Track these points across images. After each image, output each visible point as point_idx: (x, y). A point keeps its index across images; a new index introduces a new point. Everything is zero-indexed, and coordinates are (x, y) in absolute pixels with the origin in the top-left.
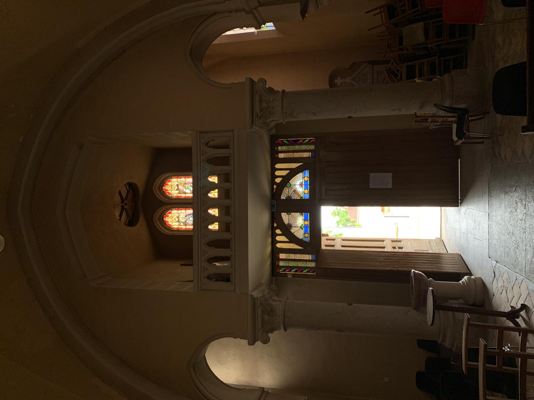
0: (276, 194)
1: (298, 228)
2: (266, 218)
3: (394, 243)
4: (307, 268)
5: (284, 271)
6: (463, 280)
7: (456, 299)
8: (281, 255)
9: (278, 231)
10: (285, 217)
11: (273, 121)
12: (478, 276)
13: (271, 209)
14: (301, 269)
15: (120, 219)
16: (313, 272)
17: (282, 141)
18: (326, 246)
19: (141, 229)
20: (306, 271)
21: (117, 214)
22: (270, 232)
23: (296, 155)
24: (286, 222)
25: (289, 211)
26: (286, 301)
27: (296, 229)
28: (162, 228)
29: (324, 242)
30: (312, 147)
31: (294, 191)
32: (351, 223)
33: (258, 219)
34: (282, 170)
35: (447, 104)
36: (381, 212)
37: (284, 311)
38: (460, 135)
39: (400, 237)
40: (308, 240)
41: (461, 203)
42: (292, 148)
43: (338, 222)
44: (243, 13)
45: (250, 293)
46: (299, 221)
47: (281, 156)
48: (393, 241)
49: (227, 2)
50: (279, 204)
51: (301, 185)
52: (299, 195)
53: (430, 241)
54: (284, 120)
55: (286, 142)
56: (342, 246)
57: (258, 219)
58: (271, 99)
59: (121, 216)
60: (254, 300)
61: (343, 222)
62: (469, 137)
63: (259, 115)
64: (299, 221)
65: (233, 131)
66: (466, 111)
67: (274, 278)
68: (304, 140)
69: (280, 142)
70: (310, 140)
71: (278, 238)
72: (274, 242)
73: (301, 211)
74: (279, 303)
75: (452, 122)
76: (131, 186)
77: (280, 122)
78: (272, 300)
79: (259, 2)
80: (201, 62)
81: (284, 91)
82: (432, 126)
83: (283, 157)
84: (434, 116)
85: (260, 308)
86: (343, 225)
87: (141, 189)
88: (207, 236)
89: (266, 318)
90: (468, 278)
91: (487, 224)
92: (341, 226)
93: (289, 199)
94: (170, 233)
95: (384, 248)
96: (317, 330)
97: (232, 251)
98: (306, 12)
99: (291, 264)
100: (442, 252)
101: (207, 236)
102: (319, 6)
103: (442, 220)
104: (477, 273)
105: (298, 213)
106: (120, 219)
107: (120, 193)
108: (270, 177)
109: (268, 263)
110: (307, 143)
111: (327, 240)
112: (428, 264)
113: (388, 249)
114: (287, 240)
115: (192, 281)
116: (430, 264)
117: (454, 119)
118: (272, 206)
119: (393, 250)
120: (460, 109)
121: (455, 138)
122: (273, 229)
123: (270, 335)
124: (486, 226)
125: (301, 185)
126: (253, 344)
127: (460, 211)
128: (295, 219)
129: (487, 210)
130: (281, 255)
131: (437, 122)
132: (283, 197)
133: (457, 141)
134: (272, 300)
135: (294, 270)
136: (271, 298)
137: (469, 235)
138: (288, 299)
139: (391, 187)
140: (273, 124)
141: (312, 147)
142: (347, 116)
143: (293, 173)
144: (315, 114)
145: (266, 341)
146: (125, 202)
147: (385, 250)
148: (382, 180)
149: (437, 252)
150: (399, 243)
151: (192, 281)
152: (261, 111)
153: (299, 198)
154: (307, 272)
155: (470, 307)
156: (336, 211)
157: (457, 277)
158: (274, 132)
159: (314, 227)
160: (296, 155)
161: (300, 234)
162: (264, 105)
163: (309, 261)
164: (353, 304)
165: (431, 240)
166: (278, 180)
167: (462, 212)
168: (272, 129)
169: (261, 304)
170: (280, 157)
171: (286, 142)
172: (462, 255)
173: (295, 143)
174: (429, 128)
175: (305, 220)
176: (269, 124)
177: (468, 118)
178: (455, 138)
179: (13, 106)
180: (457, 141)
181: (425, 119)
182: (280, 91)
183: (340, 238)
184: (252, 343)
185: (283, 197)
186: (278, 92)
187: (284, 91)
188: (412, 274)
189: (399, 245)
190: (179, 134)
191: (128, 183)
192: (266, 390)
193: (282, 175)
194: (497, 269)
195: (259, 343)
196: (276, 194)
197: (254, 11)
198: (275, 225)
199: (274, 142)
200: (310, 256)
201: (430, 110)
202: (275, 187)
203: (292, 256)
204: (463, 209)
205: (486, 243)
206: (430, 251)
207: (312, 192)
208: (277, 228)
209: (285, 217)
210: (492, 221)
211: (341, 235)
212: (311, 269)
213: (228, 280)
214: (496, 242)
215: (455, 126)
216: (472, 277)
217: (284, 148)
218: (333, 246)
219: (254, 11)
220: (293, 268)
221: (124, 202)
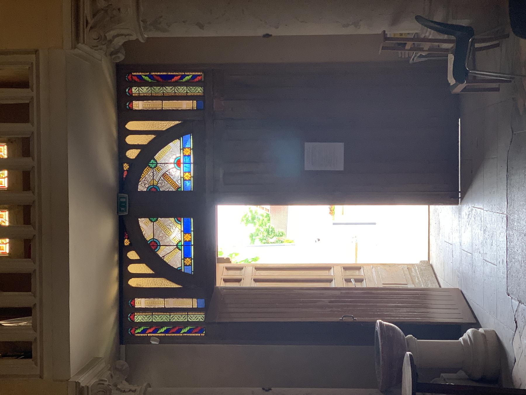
0: (126, 182)
1: (172, 248)
2: (106, 229)
3: (348, 273)
4: (188, 323)
5: (144, 332)
6: (465, 336)
7: (454, 370)
8: (137, 300)
9: (132, 255)
10: (146, 226)
11: (118, 36)
12: (490, 328)
13: (119, 210)
14: (178, 326)
17: (140, 77)
18: (226, 281)
20: (185, 330)
22: (116, 257)
23: (168, 105)
24: (148, 235)
25: (154, 215)
26: (146, 389)
27: (167, 249)
29: (221, 273)
30: (199, 90)
31: (164, 175)
32: (272, 236)
33: (89, 233)
34: (139, 133)
35: (439, 17)
36: (330, 215)
38: (461, 74)
39: (360, 261)
40: (190, 270)
41: (462, 198)
42: (158, 90)
43: (252, 236)
45: (73, 378)
47: (138, 105)
48: (346, 268)
50: (132, 204)
51: (178, 163)
52: (173, 183)
53: (410, 267)
54: (142, 35)
55: (147, 78)
56: (256, 280)
57: (89, 233)
61: (261, 236)
62: (475, 79)
63: (91, 22)
65: (36, 52)
66: (469, 31)
67: (123, 347)
68: (183, 77)
69: (136, 79)
70: (194, 77)
71: (132, 268)
72: (124, 276)
73: (177, 215)
75: (447, 50)
77: (133, 38)
78: (118, 389)
82: (415, 58)
83: (141, 108)
84: (417, 38)
86: (261, 240)
90: (474, 333)
91: (504, 235)
92: (257, 242)
93: (153, 191)
95: (330, 281)
97: (35, 296)
99: (158, 318)
100: (430, 286)
103: (431, 227)
104: (490, 323)
105: (172, 219)
108: (116, 149)
109: (112, 318)
110: (187, 81)
111: (228, 269)
112: (405, 310)
113: (338, 283)
114: (149, 271)
116: (408, 310)
117: (449, 46)
118: (120, 206)
119: (345, 285)
120: (460, 28)
121: (452, 81)
122: (122, 251)
124: (503, 239)
125: (178, 163)
127: (460, 211)
128: (167, 231)
129: (505, 210)
130: (137, 300)
131: (422, 50)
132: (142, 187)
133: (455, 86)
134: (118, 389)
135: (163, 330)
136: (115, 385)
137: (476, 255)
138: (149, 386)
139: (342, 169)
140: (119, 42)
141: (199, 90)
142: (261, 33)
143: (162, 140)
144: (201, 27)
147: (333, 285)
148: (331, 155)
149: (423, 286)
150: (357, 272)
152: (94, 15)
153: (172, 189)
154: (189, 332)
155: (477, 385)
156: (250, 214)
157: (454, 330)
158: (121, 57)
159: (203, 248)
160: (168, 105)
161: (175, 259)
163: (192, 310)
165: (413, 265)
166: (132, 154)
167: (463, 213)
171: (147, 78)
172: (464, 292)
173: (166, 80)
174: (408, 61)
175: (186, 231)
176: (111, 41)
177: (473, 43)
178: (452, 81)
180: (455, 86)
181: (400, 43)
183: (252, 265)
185: (142, 187)
188: (378, 328)
189: (357, 274)
193: (140, 143)
194: (520, 314)
196: (126, 182)
198: (127, 242)
199: (124, 77)
200: (195, 300)
201: (409, 28)
202: (126, 167)
203: (160, 303)
204: (466, 208)
205: (503, 268)
206: (410, 286)
209: (146, 226)
210: (512, 229)
211: (255, 259)
212: (196, 326)
213: (28, 355)
214: (519, 267)
215: (451, 58)
216: (481, 330)
217: (144, 90)
218: (239, 281)
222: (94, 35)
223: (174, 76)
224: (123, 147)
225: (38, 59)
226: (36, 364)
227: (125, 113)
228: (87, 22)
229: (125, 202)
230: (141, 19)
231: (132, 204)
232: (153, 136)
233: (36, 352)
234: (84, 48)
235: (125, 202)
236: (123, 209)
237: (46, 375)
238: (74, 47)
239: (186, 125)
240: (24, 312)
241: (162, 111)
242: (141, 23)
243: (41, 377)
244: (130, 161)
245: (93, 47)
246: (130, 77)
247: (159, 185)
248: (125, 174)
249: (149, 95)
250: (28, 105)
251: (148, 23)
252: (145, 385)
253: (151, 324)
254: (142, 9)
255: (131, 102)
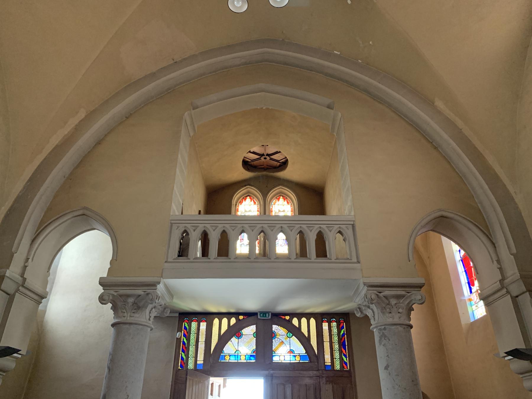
0: (278, 317)
2: (251, 305)
4: (188, 357)
5: (185, 328)
8: (205, 323)
9: (233, 321)
10: (250, 330)
13: (261, 313)
14: (186, 350)
15: (250, 152)
16: (181, 366)
17: (343, 328)
19: (240, 173)
21: (256, 149)
22: (232, 311)
23: (327, 345)
24: (245, 331)
25: (257, 335)
28: (238, 196)
30: (337, 367)
37: (136, 324)
42: (335, 339)
44: (500, 278)
45: (163, 281)
46: (242, 347)
47: (325, 326)
49: (512, 257)
52: (277, 348)
55: (342, 332)
57: (251, 293)
58: (400, 310)
59: (254, 153)
60: (154, 285)
63: (381, 295)
64: (242, 347)
67: (177, 315)
70: (346, 364)
71: (225, 321)
72: (220, 315)
74: (148, 317)
76: (284, 164)
77: (372, 322)
78: (152, 309)
79: (517, 297)
80: (431, 230)
81: (411, 327)
83: (324, 328)
85: (143, 293)
87: (282, 174)
88: (233, 230)
89: (131, 300)
93: (273, 335)
94: (234, 202)
96: (109, 368)
98: (514, 357)
99: (193, 337)
101: (233, 230)
102: (521, 376)
106: (250, 152)
107: (277, 153)
109: (196, 308)
114: (222, 332)
115: (182, 214)
118: (264, 313)
122: (236, 314)
123: (110, 305)
126: (101, 283)
130: (205, 323)
134: (152, 309)
136: (155, 307)
140: (369, 313)
141: (337, 367)
143: (305, 341)
144: (386, 368)
145: (102, 300)
146: (268, 158)
151: (182, 214)
161: (230, 348)
162: (393, 302)
164: (374, 305)
166: (295, 321)
168: (362, 312)
169: (148, 294)
170: (324, 324)
171: (342, 332)
173: (342, 344)
176: (369, 307)
179: (371, 43)
182: (411, 323)
184: (103, 283)
185: (275, 328)
186: (410, 319)
187: (411, 327)
190: (349, 203)
191: (287, 160)
192: (43, 300)
195: (101, 290)
197: (504, 291)
198: (241, 317)
199: (343, 318)
200: (202, 362)
202: (287, 318)
207: (282, 366)
208: (238, 320)
212: (185, 363)
217: (335, 330)
218: (212, 394)
219: (504, 291)
220: (188, 340)
221: (267, 157)
222: (373, 296)
223: (345, 349)
224: (300, 316)
225: (355, 263)
226: (174, 259)
227: (320, 317)
228: (380, 292)
229: (266, 317)
230: (386, 327)
231: (267, 321)
232: (307, 336)
233: (181, 259)
234: (364, 290)
235: (266, 317)
236: (263, 315)
237: (166, 264)
238: (365, 284)
239: (314, 357)
240: (205, 252)
241: (323, 342)
242: (383, 327)
243: (166, 262)
244: (290, 321)
245: (366, 295)
246: (342, 321)
247: (276, 339)
248: (283, 317)
249: (332, 334)
250: (326, 256)
251: (384, 331)
252: (153, 327)
253: (189, 333)
254: (393, 327)
255: (327, 322)
